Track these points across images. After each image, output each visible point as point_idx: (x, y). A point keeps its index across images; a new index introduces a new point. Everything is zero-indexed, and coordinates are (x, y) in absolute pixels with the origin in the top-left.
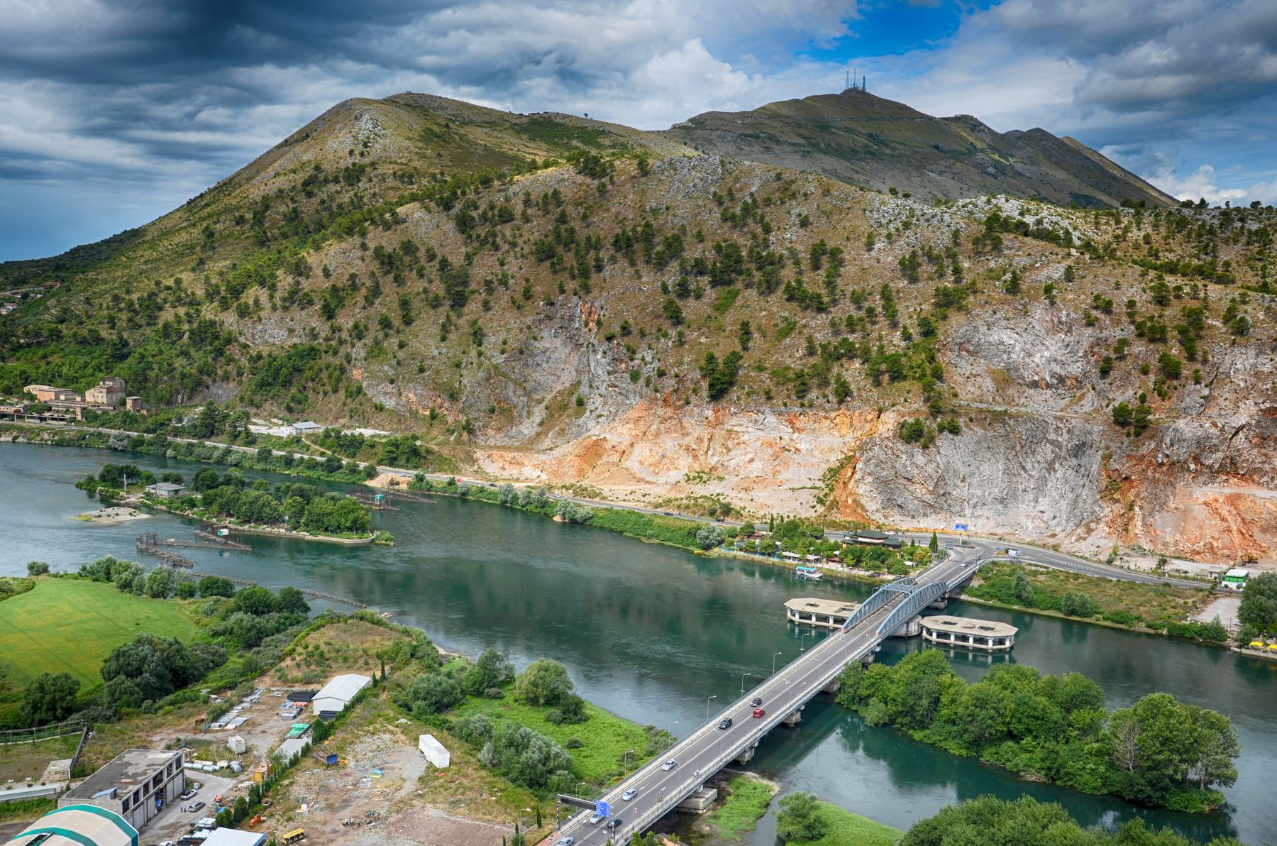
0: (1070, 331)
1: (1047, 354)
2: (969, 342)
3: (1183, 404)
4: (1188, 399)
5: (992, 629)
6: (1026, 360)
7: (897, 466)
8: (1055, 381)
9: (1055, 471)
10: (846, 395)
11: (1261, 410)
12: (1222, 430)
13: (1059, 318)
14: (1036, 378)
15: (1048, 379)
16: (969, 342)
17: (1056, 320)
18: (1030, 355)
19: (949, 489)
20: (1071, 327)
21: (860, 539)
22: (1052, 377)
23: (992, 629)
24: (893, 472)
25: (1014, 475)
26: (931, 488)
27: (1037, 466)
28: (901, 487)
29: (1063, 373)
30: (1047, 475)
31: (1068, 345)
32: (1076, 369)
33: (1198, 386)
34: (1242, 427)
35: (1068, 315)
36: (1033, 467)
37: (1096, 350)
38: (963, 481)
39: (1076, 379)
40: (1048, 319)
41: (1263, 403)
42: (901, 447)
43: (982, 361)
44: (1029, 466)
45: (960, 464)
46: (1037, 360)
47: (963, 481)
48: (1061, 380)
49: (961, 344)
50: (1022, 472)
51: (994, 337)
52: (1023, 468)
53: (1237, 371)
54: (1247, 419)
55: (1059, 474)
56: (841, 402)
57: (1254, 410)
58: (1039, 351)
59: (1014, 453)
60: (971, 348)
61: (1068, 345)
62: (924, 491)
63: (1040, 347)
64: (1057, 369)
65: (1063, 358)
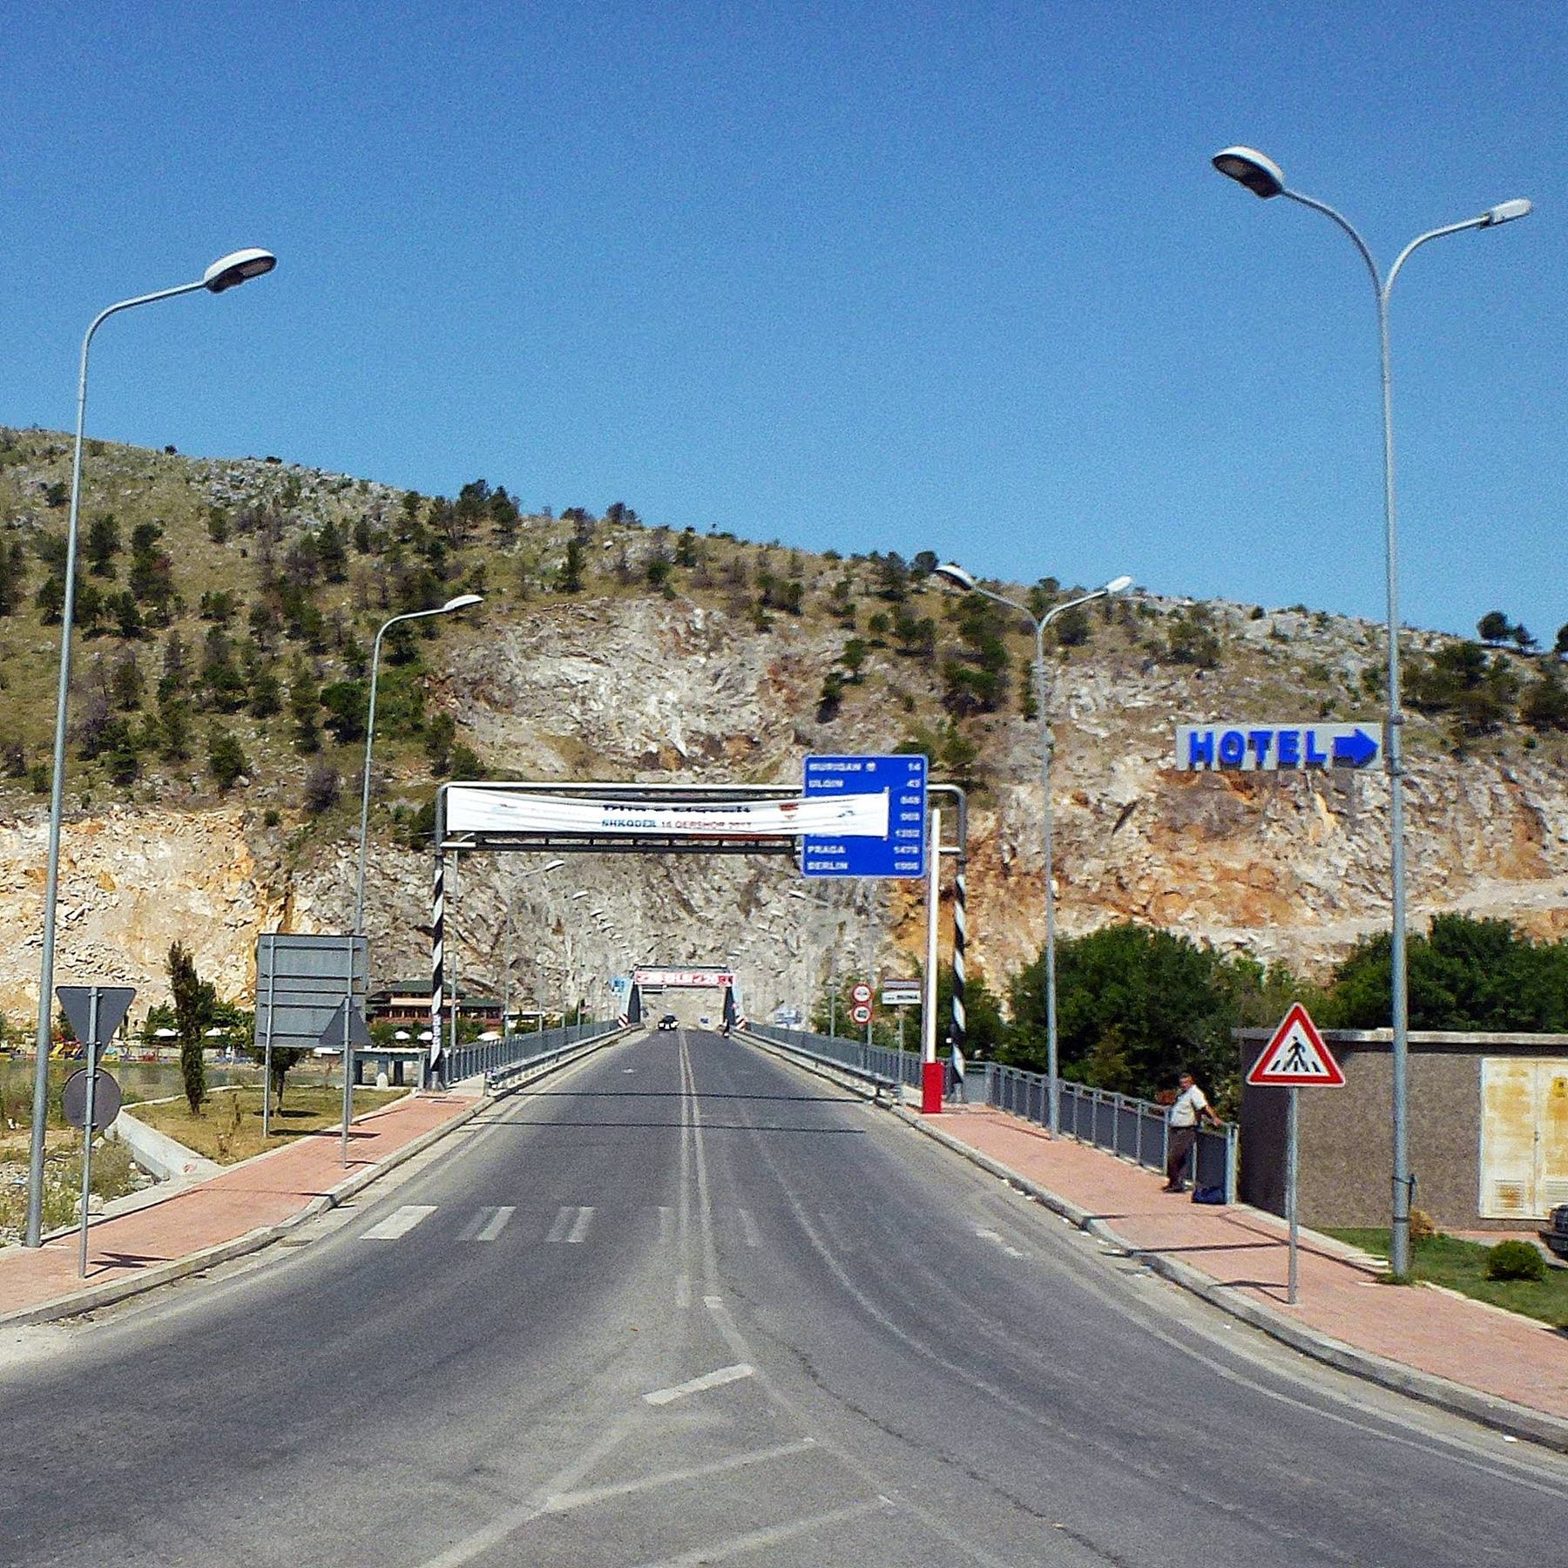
0: (716, 647)
1: (671, 696)
2: (491, 680)
3: (1010, 761)
4: (1017, 750)
5: (1278, 1062)
6: (625, 710)
7: (396, 902)
8: (698, 750)
9: (760, 905)
10: (239, 771)
11: (1161, 773)
12: (1097, 811)
13: (689, 623)
14: (653, 748)
15: (682, 747)
16: (491, 680)
17: (681, 628)
18: (635, 701)
19: (528, 953)
20: (718, 638)
21: (395, 1001)
22: (690, 741)
23: (1278, 1062)
24: (385, 919)
25: (666, 921)
26: (486, 949)
27: (713, 895)
28: (411, 951)
29: (716, 730)
30: (742, 918)
31: (717, 676)
32: (747, 717)
33: (1032, 725)
34: (1133, 805)
35: (708, 616)
36: (708, 901)
37: (783, 677)
38: (558, 930)
39: (749, 740)
40: (663, 626)
41: (1162, 757)
42: (400, 861)
43: (524, 720)
44: (697, 900)
45: (545, 893)
46: (651, 708)
47: (558, 930)
48: (713, 745)
49: (475, 683)
50: (683, 914)
51: (544, 671)
52: (686, 904)
53: (1083, 709)
54: (1138, 790)
55: (774, 909)
56: (225, 788)
57: (1148, 772)
58: (654, 691)
59: (661, 871)
60: (497, 694)
61: (717, 676)
62: (469, 956)
63: (654, 682)
64: (702, 724)
65: (710, 702)
